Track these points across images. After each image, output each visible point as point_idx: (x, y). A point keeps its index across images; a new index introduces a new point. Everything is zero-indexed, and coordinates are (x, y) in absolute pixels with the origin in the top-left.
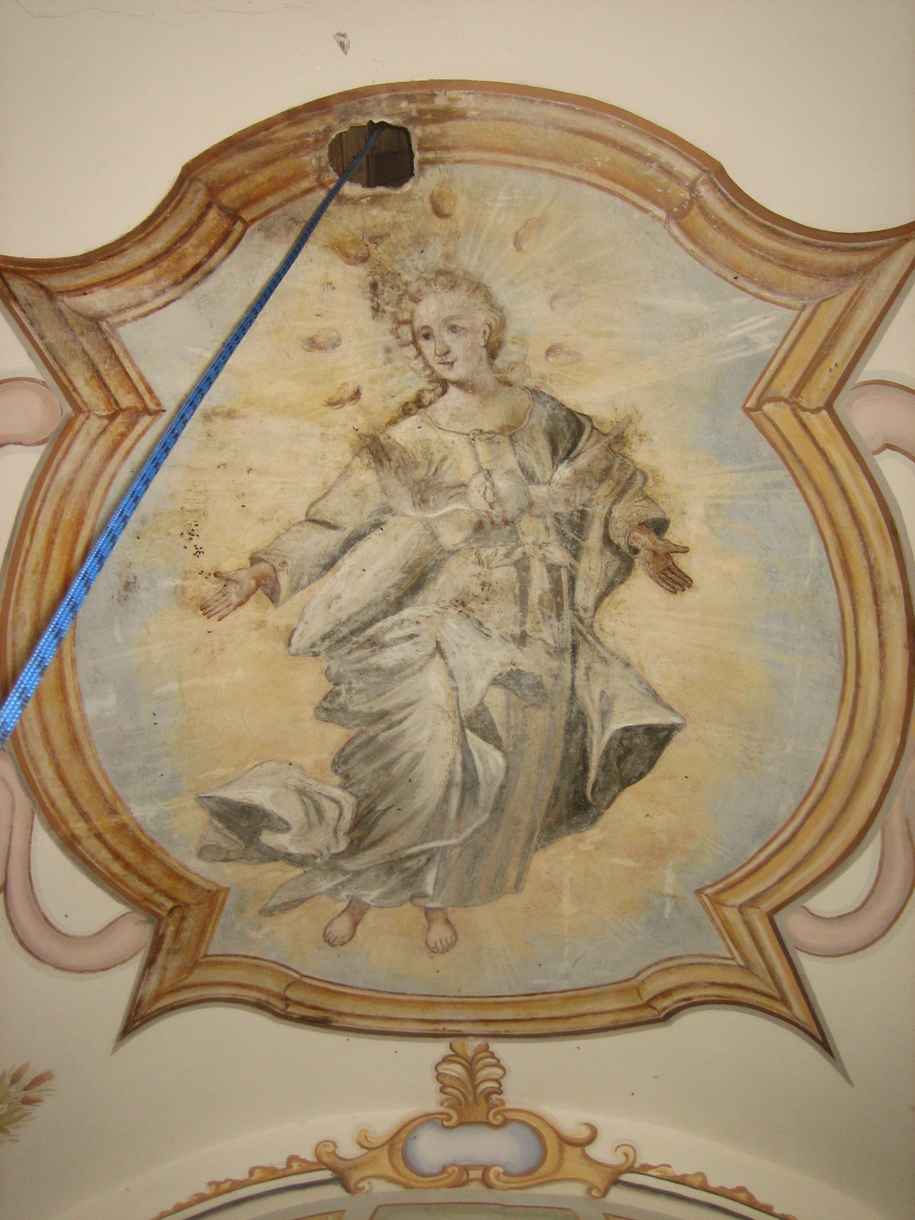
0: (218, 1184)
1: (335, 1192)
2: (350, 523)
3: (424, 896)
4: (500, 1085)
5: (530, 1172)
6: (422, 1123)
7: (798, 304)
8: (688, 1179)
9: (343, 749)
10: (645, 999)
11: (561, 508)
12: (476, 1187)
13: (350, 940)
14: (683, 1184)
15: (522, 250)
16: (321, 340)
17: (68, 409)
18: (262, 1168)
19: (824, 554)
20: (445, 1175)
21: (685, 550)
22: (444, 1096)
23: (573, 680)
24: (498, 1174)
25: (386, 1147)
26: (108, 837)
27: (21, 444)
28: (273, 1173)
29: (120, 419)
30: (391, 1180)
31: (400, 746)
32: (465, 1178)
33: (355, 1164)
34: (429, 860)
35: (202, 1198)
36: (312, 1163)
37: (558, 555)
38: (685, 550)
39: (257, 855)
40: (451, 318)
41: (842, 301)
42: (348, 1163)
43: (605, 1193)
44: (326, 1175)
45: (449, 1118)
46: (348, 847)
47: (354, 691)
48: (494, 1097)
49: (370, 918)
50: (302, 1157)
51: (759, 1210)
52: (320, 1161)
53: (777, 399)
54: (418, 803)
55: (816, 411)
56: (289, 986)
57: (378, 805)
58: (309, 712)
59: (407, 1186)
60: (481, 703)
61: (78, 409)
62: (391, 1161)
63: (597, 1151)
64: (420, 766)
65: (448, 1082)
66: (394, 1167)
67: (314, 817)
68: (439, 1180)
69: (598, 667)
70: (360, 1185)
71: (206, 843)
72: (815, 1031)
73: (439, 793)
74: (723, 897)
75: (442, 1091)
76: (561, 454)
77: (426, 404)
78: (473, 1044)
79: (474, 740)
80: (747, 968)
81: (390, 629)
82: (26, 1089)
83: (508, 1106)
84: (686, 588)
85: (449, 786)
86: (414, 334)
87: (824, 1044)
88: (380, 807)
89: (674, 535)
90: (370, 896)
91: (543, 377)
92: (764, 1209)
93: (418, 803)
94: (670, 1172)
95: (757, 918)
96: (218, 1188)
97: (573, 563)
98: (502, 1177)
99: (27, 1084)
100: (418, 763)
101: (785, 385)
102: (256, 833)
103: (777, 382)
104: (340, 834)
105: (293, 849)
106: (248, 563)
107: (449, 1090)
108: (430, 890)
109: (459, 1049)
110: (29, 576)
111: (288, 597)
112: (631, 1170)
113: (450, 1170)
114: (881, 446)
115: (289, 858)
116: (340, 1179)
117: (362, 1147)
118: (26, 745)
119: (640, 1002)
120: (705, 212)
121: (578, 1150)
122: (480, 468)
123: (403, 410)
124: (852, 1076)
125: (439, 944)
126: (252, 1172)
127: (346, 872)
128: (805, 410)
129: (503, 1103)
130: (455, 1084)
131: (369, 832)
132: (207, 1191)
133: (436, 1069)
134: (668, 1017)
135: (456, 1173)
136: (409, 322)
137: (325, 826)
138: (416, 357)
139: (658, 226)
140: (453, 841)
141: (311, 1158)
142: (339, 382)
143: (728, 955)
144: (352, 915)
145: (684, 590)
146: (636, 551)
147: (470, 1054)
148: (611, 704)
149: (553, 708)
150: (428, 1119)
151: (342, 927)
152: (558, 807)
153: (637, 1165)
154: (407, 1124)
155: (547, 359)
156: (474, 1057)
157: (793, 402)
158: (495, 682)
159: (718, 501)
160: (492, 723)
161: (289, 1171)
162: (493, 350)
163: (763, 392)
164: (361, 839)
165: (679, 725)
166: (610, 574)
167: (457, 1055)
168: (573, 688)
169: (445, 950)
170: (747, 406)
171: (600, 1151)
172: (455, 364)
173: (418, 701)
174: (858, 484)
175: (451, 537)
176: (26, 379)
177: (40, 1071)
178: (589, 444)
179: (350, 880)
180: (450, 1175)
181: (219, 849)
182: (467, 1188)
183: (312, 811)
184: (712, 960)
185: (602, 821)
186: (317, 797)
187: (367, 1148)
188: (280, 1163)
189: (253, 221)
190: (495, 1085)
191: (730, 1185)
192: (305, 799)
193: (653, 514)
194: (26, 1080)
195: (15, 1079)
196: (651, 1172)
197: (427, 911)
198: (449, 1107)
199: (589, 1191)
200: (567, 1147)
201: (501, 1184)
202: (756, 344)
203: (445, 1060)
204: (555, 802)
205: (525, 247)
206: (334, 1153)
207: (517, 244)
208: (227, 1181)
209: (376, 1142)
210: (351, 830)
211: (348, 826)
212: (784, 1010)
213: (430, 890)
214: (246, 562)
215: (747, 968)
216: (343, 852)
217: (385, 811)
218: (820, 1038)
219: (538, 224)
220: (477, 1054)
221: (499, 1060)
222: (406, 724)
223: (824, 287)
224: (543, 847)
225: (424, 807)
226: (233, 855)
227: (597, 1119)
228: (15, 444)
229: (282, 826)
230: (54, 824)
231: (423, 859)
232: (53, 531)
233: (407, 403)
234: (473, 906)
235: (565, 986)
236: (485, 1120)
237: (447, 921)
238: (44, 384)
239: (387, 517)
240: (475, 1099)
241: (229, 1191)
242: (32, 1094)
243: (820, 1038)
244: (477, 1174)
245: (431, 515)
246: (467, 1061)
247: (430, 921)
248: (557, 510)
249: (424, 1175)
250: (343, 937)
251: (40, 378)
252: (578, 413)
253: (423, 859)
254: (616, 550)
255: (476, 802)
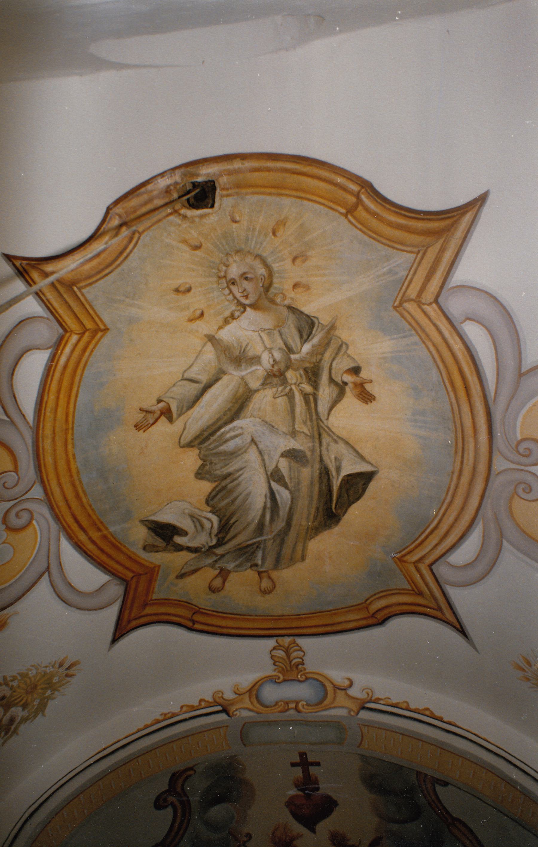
0: (165, 714)
1: (223, 717)
2: (204, 378)
3: (256, 565)
4: (303, 660)
5: (320, 703)
6: (265, 681)
7: (416, 250)
8: (400, 705)
9: (210, 493)
10: (371, 612)
11: (308, 365)
12: (292, 712)
13: (222, 589)
14: (398, 707)
15: (277, 236)
16: (182, 289)
17: (61, 331)
18: (187, 706)
19: (440, 377)
20: (277, 706)
21: (371, 381)
22: (276, 667)
23: (321, 452)
24: (303, 705)
25: (248, 694)
26: (98, 542)
27: (39, 349)
28: (193, 708)
29: (87, 334)
30: (250, 710)
31: (240, 489)
32: (287, 708)
33: (232, 703)
34: (257, 547)
35: (158, 722)
36: (211, 703)
37: (308, 389)
38: (371, 381)
39: (172, 548)
40: (244, 273)
41: (438, 246)
42: (229, 702)
43: (358, 713)
44: (219, 708)
45: (279, 678)
46: (217, 543)
47: (213, 464)
48: (300, 666)
49: (233, 577)
50: (206, 699)
51: (436, 719)
52: (215, 701)
53: (409, 300)
54: (250, 518)
55: (430, 304)
56: (194, 613)
57: (230, 520)
58: (192, 476)
59: (258, 713)
60: (277, 466)
61: (65, 331)
62: (250, 701)
63: (352, 692)
64: (249, 500)
65: (276, 659)
66: (252, 703)
67: (199, 528)
68: (274, 709)
69: (333, 444)
70: (235, 713)
71: (147, 543)
72: (458, 626)
73: (260, 513)
74: (405, 558)
75: (274, 664)
76: (305, 337)
77: (236, 317)
78: (287, 641)
79: (274, 485)
80: (413, 590)
81: (228, 432)
82: (67, 669)
83: (307, 671)
84: (373, 401)
85: (265, 508)
86: (227, 283)
87: (462, 632)
88: (232, 522)
89: (364, 374)
90: (230, 566)
91: (292, 299)
92: (439, 719)
93: (250, 518)
94: (390, 702)
95: (424, 568)
96: (165, 716)
97: (315, 392)
98: (305, 707)
99: (67, 667)
100: (247, 499)
101: (412, 292)
102: (171, 537)
103: (409, 292)
104: (213, 536)
105: (190, 545)
106: (156, 402)
107: (277, 663)
108: (260, 562)
109: (281, 643)
110: (48, 414)
111: (177, 419)
112: (370, 701)
113: (279, 704)
114: (464, 319)
115: (189, 549)
116: (225, 711)
117: (236, 693)
118: (53, 498)
119: (369, 615)
120: (367, 209)
121: (343, 692)
122: (266, 348)
123: (225, 322)
124: (478, 647)
125: (266, 590)
126: (182, 707)
127: (216, 555)
128: (424, 304)
129: (305, 669)
130: (281, 660)
131: (227, 533)
132: (160, 718)
133: (271, 654)
134: (382, 622)
135: (282, 706)
136: (225, 277)
137: (205, 532)
138: (229, 294)
139: (342, 218)
140: (270, 537)
141: (210, 699)
142: (192, 310)
143: (410, 588)
144: (222, 577)
145: (371, 402)
146: (346, 384)
147: (286, 645)
148: (340, 463)
149: (312, 467)
150: (272, 680)
151: (218, 582)
152: (319, 517)
153: (373, 698)
154: (258, 682)
155: (293, 291)
156: (289, 646)
157: (419, 304)
158: (283, 455)
159: (384, 355)
160: (283, 476)
161: (200, 707)
162: (267, 289)
163: (402, 297)
164: (223, 538)
165: (375, 471)
166: (334, 396)
167: (281, 646)
168: (321, 457)
169: (270, 592)
170: (395, 305)
171: (354, 692)
172: (249, 296)
173: (245, 467)
174: (455, 340)
175: (254, 384)
176: (39, 317)
177: (74, 660)
178: (318, 332)
179: (219, 559)
180: (279, 707)
181: (154, 546)
182: (288, 713)
183: (198, 524)
184: (402, 592)
185: (342, 523)
186: (200, 518)
187: (238, 694)
188: (196, 704)
189: (144, 231)
190: (300, 660)
191: (421, 707)
192: (194, 519)
193: (353, 365)
194: (66, 665)
195: (61, 665)
196: (381, 702)
197: (259, 573)
198: (279, 672)
199: (349, 712)
200: (338, 691)
201: (304, 710)
202: (396, 273)
203: (274, 648)
204: (317, 515)
205: (277, 234)
206: (222, 697)
207: (274, 233)
208: (169, 713)
209: (242, 691)
210: (218, 533)
211: (216, 532)
212: (438, 614)
213: (260, 562)
214: (154, 401)
215: (420, 594)
216: (215, 545)
217: (234, 523)
218: (461, 630)
219: (282, 223)
220: (291, 644)
221: (301, 648)
222: (240, 479)
223: (428, 240)
224: (313, 537)
225: (253, 520)
226: (160, 549)
227: (354, 676)
228: (36, 349)
229: (183, 533)
230: (71, 538)
231: (255, 546)
232: (59, 392)
233: (227, 318)
234: (281, 569)
235: (331, 608)
236: (297, 679)
237: (270, 577)
238: (48, 319)
239: (222, 375)
240: (291, 668)
241: (171, 717)
242: (70, 672)
243: (461, 630)
244: (292, 705)
245: (243, 373)
246: (285, 649)
247: (261, 578)
248: (305, 366)
249: (267, 707)
250: (219, 588)
251: (45, 316)
252: (311, 316)
253: (255, 546)
254: (336, 384)
255: (278, 515)
